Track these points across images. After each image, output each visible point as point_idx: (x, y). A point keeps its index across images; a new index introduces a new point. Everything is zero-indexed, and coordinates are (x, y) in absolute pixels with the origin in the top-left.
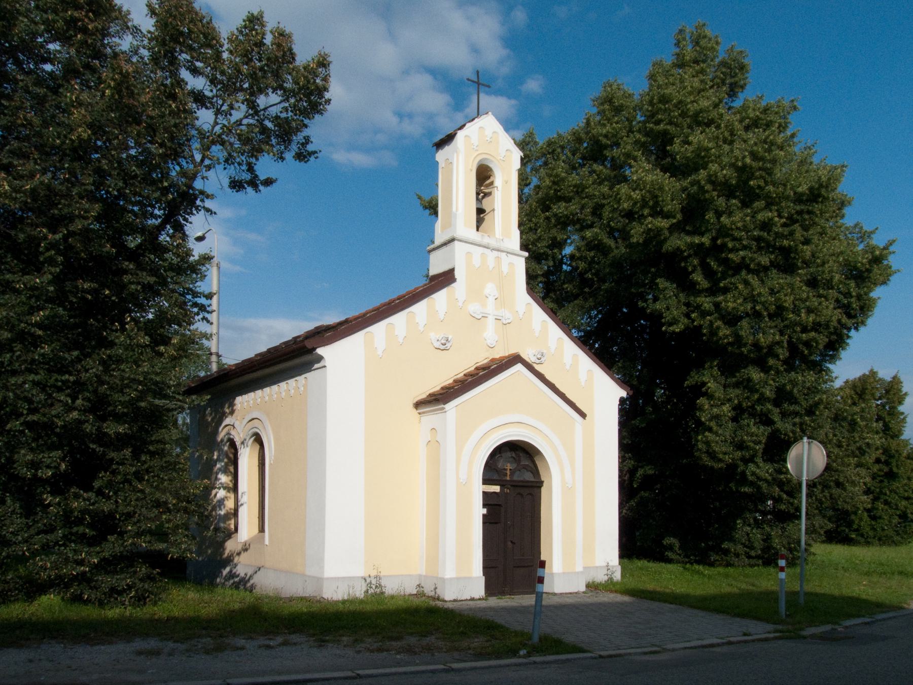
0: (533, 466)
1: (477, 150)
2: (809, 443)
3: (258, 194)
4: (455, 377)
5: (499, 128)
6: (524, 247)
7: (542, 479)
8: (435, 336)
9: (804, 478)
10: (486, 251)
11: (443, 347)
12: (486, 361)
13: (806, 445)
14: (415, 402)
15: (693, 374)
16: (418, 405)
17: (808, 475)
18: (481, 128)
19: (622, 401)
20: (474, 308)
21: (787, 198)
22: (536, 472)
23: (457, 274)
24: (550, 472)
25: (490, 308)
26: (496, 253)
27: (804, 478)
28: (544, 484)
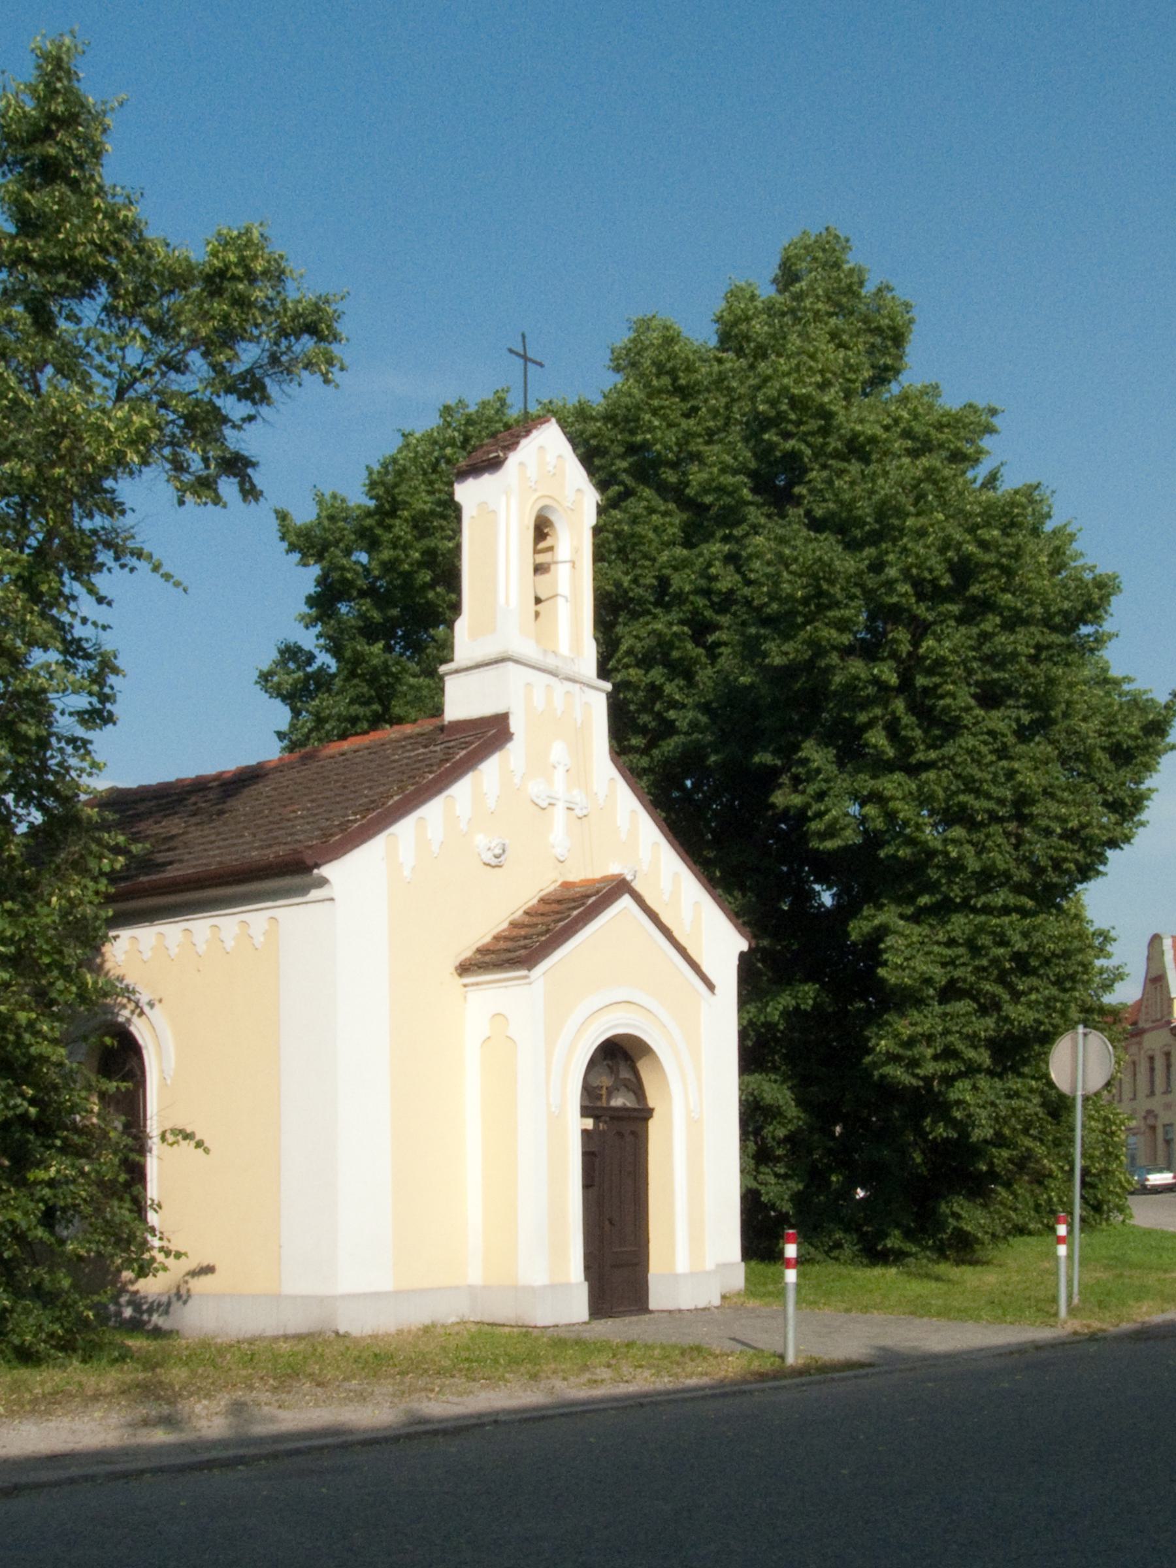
0: (634, 1080)
1: (535, 490)
2: (1085, 1035)
3: (1109, 876)
4: (512, 918)
5: (566, 448)
6: (604, 672)
7: (651, 1104)
8: (483, 842)
9: (1079, 1093)
10: (553, 680)
11: (494, 862)
12: (552, 888)
13: (1080, 1037)
14: (457, 963)
15: (867, 911)
16: (464, 969)
17: (1084, 1089)
18: (541, 448)
19: (742, 956)
20: (536, 788)
21: (861, 498)
22: (638, 1089)
23: (514, 725)
24: (668, 1085)
25: (559, 785)
26: (569, 685)
27: (1079, 1093)
28: (655, 1114)
